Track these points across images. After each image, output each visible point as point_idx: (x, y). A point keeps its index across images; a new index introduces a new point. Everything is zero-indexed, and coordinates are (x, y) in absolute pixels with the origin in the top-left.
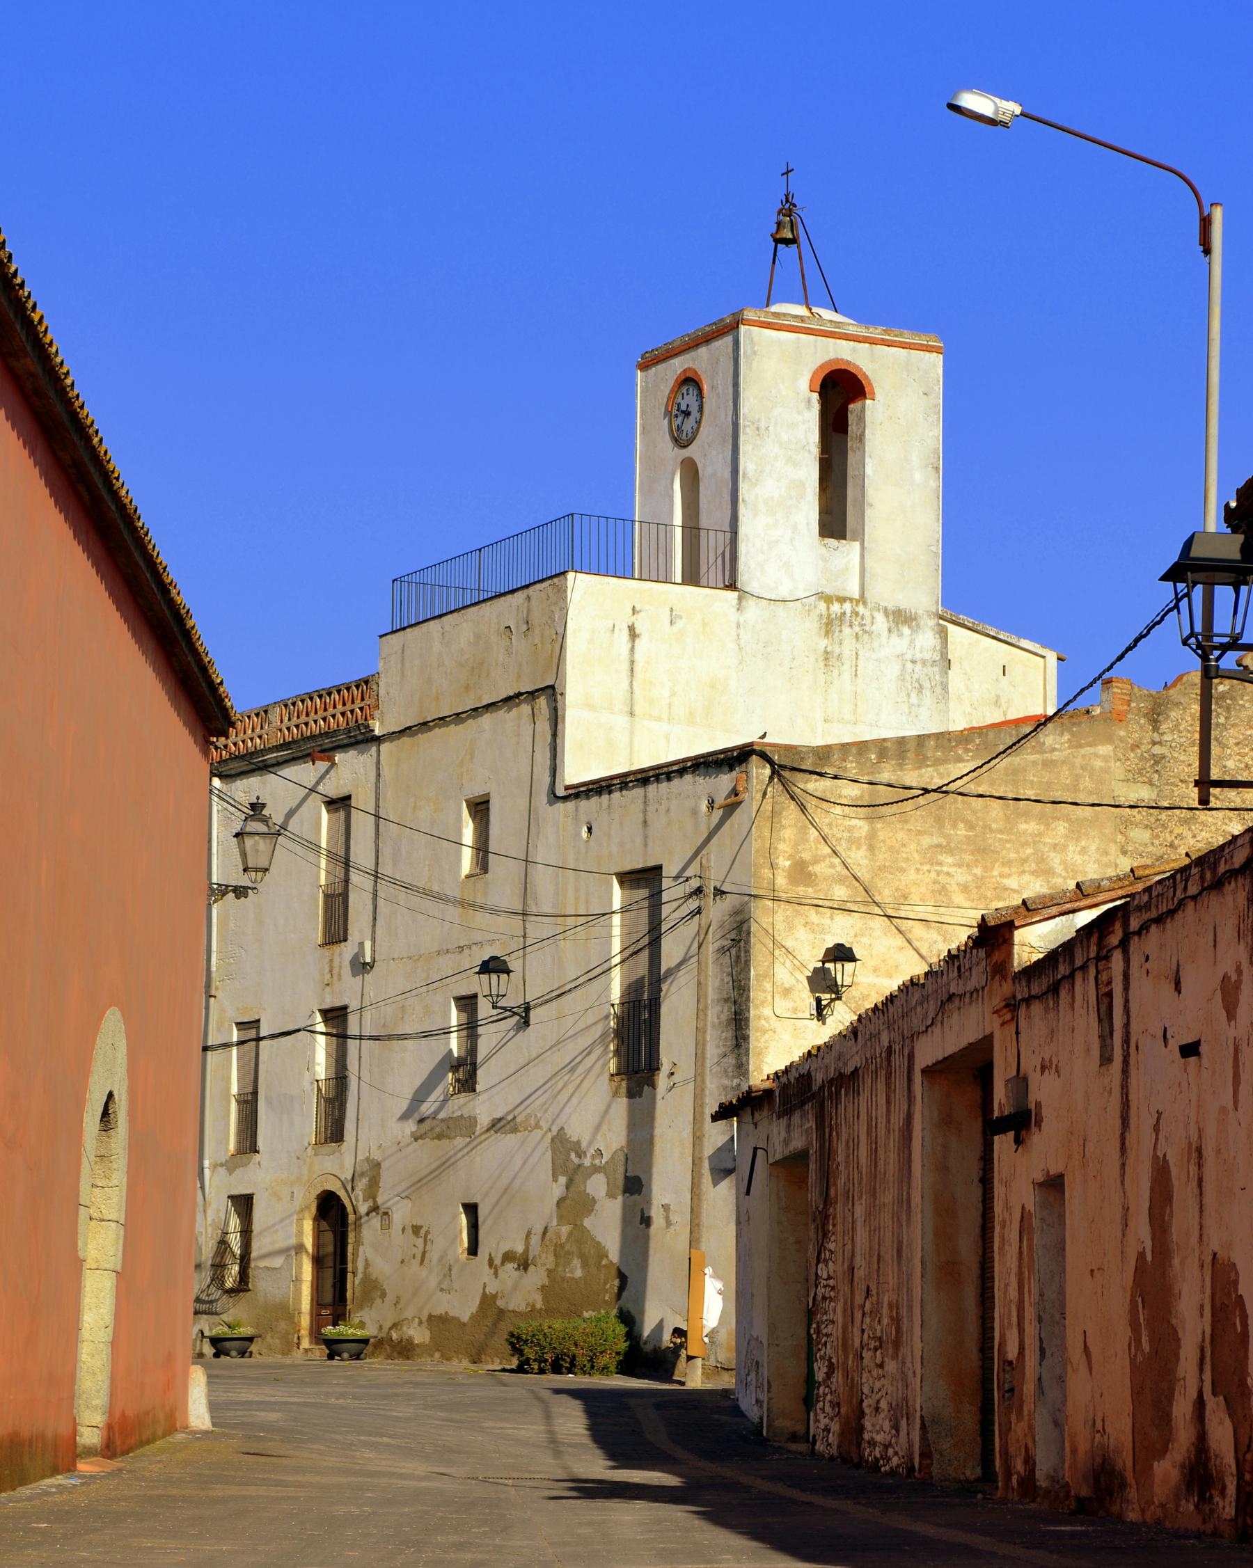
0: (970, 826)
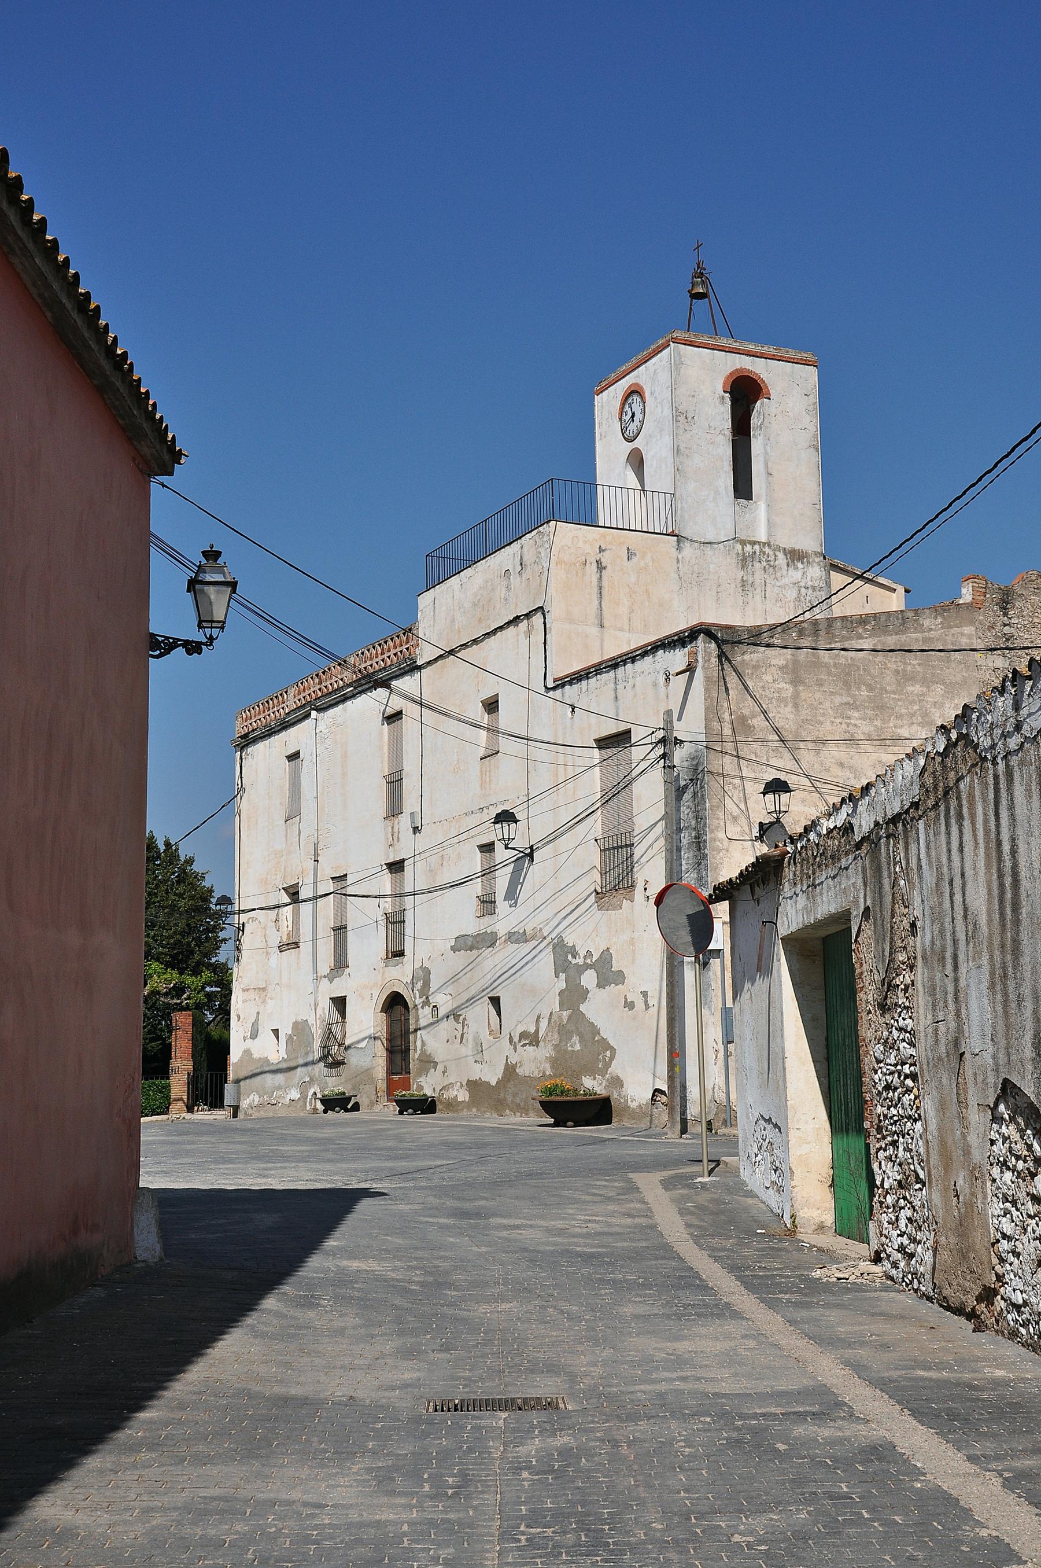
0: (871, 689)
